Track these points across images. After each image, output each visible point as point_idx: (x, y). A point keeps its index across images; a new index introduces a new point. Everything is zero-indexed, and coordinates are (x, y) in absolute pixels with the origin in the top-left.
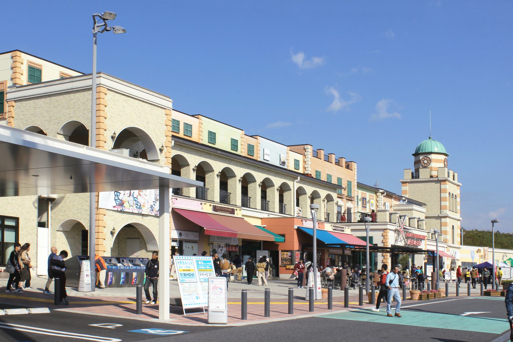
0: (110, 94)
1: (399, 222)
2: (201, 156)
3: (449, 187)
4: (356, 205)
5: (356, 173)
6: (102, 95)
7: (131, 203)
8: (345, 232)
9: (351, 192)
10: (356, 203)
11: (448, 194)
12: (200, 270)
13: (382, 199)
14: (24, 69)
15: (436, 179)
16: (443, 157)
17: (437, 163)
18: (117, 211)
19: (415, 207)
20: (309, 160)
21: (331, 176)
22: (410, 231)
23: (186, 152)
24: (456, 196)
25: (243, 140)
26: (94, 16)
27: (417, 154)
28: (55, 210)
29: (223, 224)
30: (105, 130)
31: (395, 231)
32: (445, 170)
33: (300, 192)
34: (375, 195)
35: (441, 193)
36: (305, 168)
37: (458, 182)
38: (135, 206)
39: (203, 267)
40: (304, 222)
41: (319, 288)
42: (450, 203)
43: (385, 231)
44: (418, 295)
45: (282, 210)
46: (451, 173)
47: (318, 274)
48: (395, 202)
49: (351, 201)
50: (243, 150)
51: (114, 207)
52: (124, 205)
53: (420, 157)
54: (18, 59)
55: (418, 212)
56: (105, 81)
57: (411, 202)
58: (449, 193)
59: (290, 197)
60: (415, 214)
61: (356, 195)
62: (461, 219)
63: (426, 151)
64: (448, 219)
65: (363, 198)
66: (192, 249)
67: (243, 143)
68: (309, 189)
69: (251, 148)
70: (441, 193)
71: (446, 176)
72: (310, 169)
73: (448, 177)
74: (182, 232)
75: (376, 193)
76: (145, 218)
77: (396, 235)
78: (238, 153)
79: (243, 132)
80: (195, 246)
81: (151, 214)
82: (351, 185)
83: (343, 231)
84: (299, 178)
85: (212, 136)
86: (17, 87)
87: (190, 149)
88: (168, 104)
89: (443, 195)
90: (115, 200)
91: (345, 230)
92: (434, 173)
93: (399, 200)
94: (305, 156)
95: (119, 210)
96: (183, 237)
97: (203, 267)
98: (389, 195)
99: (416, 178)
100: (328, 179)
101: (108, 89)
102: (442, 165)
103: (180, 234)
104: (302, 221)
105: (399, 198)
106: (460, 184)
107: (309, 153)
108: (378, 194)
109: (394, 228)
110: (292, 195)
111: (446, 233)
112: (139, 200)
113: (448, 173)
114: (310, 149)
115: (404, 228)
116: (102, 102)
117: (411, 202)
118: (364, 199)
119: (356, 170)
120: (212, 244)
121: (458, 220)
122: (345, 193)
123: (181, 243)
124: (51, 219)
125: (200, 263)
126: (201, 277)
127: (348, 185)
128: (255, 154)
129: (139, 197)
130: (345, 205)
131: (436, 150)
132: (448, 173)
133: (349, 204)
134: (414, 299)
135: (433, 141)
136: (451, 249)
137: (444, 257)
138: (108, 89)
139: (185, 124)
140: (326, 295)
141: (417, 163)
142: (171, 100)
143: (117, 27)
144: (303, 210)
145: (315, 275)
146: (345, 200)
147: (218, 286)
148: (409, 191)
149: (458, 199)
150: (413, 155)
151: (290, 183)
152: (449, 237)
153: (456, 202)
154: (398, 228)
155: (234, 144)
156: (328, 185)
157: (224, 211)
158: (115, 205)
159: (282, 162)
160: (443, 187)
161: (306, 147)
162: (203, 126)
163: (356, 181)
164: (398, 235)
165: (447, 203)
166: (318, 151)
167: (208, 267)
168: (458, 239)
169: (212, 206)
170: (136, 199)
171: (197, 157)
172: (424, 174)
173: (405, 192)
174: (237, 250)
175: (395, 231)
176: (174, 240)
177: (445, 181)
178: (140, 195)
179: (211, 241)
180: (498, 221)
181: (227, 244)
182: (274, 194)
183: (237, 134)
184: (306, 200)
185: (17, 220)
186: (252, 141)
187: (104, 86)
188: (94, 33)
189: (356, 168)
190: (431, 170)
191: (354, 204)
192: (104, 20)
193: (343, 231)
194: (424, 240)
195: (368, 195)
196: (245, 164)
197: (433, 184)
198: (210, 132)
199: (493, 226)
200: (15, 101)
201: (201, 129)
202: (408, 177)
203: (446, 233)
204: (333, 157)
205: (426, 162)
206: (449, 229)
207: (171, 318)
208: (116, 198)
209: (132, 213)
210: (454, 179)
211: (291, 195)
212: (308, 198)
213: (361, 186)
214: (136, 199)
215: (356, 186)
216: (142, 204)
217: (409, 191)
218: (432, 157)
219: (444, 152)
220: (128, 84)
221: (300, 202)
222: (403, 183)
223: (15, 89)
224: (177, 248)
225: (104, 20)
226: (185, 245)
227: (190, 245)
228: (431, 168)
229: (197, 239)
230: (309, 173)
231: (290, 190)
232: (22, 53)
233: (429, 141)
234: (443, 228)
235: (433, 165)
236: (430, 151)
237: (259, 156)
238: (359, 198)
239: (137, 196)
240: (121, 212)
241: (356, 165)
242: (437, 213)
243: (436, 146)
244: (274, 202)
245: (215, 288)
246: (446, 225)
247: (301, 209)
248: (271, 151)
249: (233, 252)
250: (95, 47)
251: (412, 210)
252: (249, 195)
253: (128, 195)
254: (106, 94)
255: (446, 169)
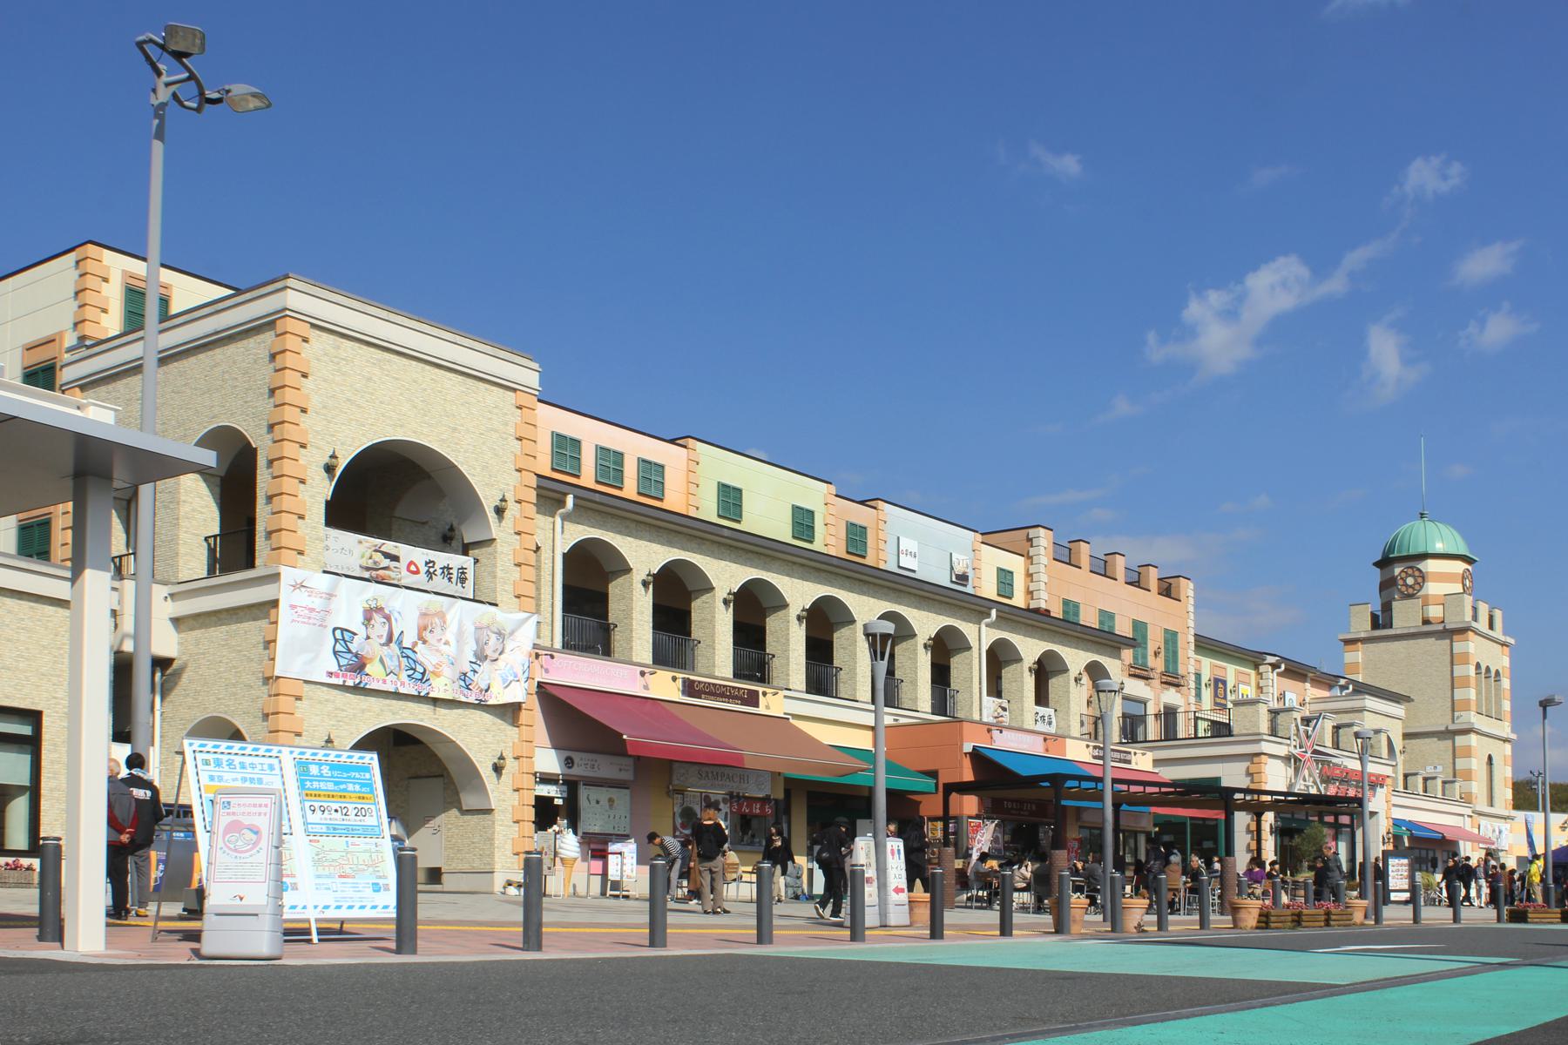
0: (320, 341)
1: (1298, 735)
2: (670, 544)
3: (1475, 648)
4: (1192, 700)
5: (1191, 609)
6: (291, 342)
7: (392, 664)
8: (1133, 766)
9: (1175, 662)
10: (1193, 692)
11: (1472, 670)
12: (307, 794)
13: (1275, 683)
14: (113, 295)
15: (1440, 627)
16: (1460, 567)
17: (1442, 582)
18: (343, 688)
19: (1370, 702)
20: (1042, 569)
21: (1111, 616)
22: (1334, 760)
23: (620, 533)
24: (1497, 673)
25: (832, 510)
26: (140, 45)
27: (1385, 563)
28: (175, 695)
29: (720, 729)
30: (303, 446)
31: (1287, 759)
32: (1462, 601)
33: (999, 658)
34: (1253, 673)
35: (1452, 664)
36: (1030, 593)
37: (1505, 633)
38: (404, 676)
39: (331, 786)
40: (995, 733)
41: (898, 890)
42: (1479, 693)
43: (1256, 760)
44: (1255, 913)
45: (941, 703)
46: (1483, 609)
47: (895, 845)
48: (1312, 692)
49: (1177, 686)
50: (832, 541)
51: (330, 674)
52: (368, 669)
53: (1396, 569)
54: (90, 266)
55: (1379, 717)
56: (299, 298)
57: (1361, 689)
58: (1478, 666)
59: (970, 670)
60: (1369, 723)
61: (1192, 670)
62: (1514, 736)
63: (1412, 552)
64: (1473, 736)
65: (1217, 681)
66: (611, 806)
67: (831, 520)
68: (1030, 648)
69: (856, 536)
70: (1452, 664)
71: (1468, 617)
72: (1044, 595)
73: (1475, 618)
74: (576, 756)
75: (1256, 667)
76: (442, 711)
77: (1291, 771)
78: (818, 545)
79: (833, 489)
80: (622, 798)
81: (463, 699)
82: (1175, 643)
83: (1129, 762)
84: (994, 612)
85: (730, 498)
86: (88, 347)
87: (633, 525)
88: (528, 375)
89: (1459, 671)
90: (335, 653)
91: (1134, 759)
92: (1435, 612)
93: (1330, 687)
94: (1030, 558)
95: (350, 683)
96: (576, 771)
97: (331, 786)
98: (1296, 672)
99: (1384, 627)
100: (1101, 623)
101: (313, 325)
102: (1458, 588)
103: (569, 762)
104: (989, 731)
105: (1327, 681)
106: (1511, 641)
107: (1042, 551)
108: (1262, 669)
109: (1282, 751)
110: (976, 662)
111: (1468, 775)
112: (419, 657)
113: (1475, 609)
114: (1044, 538)
115: (1315, 752)
116: (289, 360)
117: (1361, 689)
118: (1219, 683)
119: (1191, 601)
120: (681, 792)
121: (1505, 740)
122: (1157, 664)
123: (571, 786)
124: (163, 720)
125: (314, 770)
126: (311, 818)
127: (1166, 642)
128: (871, 553)
129: (420, 647)
130: (1155, 697)
131: (1439, 547)
132: (1475, 609)
133: (1171, 697)
134: (1242, 925)
135: (1430, 525)
136: (1484, 821)
137: (1461, 843)
138: (313, 325)
139: (643, 463)
140: (924, 913)
141: (1387, 585)
142: (535, 366)
143: (238, 89)
144: (1014, 706)
145: (879, 849)
146: (1156, 683)
147: (247, 821)
148: (1360, 662)
149: (1506, 683)
150: (1377, 564)
151: (968, 629)
152: (1478, 787)
153: (1498, 689)
154: (1296, 752)
155: (803, 521)
156: (1104, 639)
157: (722, 695)
158: (335, 668)
159: (958, 576)
160: (1459, 647)
161: (1032, 532)
162: (699, 469)
163: (1192, 632)
164: (1297, 770)
165: (1472, 694)
166: (1071, 546)
167: (351, 787)
168: (1505, 794)
169: (680, 682)
170: (409, 653)
171: (655, 547)
172: (1405, 615)
173: (1354, 667)
174: (768, 811)
175: (1287, 759)
176: (546, 779)
177: (1463, 631)
178: (425, 642)
179: (676, 782)
180: (1557, 698)
181: (731, 794)
182: (914, 660)
183: (814, 495)
184: (1021, 681)
185: (34, 717)
186: (861, 515)
187: (299, 316)
188: (156, 103)
189: (1191, 593)
190: (1425, 604)
191: (1187, 697)
192: (179, 56)
193: (1129, 762)
194: (1382, 786)
195: (1231, 671)
196: (818, 570)
197: (1432, 640)
198: (724, 486)
199: (1545, 717)
200: (83, 388)
201: (692, 477)
202: (1362, 626)
203: (1468, 775)
204: (1153, 574)
205: (1410, 581)
206: (1477, 765)
207: (108, 944)
208: (339, 648)
209: (396, 695)
210: (1491, 627)
211: (970, 665)
212: (1027, 673)
213: (1205, 645)
214: (409, 653)
215: (1192, 646)
216: (430, 668)
217: (1360, 662)
218: (1430, 566)
219: (1463, 550)
220: (384, 314)
221: (175, 367)
222: (1348, 642)
223: (84, 352)
224: (558, 802)
225: (179, 56)
226: (584, 793)
227: (603, 794)
228: (1426, 597)
229: (627, 775)
230: (1043, 605)
231: (969, 648)
232: (106, 251)
233: (1419, 524)
234: (1461, 764)
235: (1433, 588)
236: (1421, 550)
237: (882, 556)
238: (1205, 679)
239: (415, 644)
240: (358, 690)
241: (1191, 585)
242: (1441, 722)
243: (1442, 538)
244: (914, 683)
245: (235, 827)
246: (1468, 751)
247: (1005, 705)
248: (917, 543)
249: (756, 816)
250: (158, 147)
251: (1361, 710)
252: (836, 663)
253: (383, 640)
254: (305, 340)
255: (1468, 600)
